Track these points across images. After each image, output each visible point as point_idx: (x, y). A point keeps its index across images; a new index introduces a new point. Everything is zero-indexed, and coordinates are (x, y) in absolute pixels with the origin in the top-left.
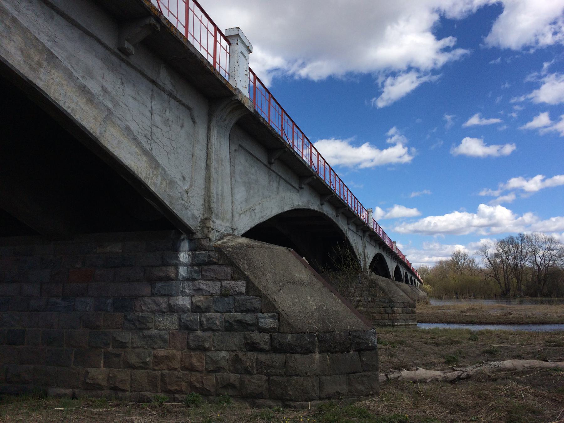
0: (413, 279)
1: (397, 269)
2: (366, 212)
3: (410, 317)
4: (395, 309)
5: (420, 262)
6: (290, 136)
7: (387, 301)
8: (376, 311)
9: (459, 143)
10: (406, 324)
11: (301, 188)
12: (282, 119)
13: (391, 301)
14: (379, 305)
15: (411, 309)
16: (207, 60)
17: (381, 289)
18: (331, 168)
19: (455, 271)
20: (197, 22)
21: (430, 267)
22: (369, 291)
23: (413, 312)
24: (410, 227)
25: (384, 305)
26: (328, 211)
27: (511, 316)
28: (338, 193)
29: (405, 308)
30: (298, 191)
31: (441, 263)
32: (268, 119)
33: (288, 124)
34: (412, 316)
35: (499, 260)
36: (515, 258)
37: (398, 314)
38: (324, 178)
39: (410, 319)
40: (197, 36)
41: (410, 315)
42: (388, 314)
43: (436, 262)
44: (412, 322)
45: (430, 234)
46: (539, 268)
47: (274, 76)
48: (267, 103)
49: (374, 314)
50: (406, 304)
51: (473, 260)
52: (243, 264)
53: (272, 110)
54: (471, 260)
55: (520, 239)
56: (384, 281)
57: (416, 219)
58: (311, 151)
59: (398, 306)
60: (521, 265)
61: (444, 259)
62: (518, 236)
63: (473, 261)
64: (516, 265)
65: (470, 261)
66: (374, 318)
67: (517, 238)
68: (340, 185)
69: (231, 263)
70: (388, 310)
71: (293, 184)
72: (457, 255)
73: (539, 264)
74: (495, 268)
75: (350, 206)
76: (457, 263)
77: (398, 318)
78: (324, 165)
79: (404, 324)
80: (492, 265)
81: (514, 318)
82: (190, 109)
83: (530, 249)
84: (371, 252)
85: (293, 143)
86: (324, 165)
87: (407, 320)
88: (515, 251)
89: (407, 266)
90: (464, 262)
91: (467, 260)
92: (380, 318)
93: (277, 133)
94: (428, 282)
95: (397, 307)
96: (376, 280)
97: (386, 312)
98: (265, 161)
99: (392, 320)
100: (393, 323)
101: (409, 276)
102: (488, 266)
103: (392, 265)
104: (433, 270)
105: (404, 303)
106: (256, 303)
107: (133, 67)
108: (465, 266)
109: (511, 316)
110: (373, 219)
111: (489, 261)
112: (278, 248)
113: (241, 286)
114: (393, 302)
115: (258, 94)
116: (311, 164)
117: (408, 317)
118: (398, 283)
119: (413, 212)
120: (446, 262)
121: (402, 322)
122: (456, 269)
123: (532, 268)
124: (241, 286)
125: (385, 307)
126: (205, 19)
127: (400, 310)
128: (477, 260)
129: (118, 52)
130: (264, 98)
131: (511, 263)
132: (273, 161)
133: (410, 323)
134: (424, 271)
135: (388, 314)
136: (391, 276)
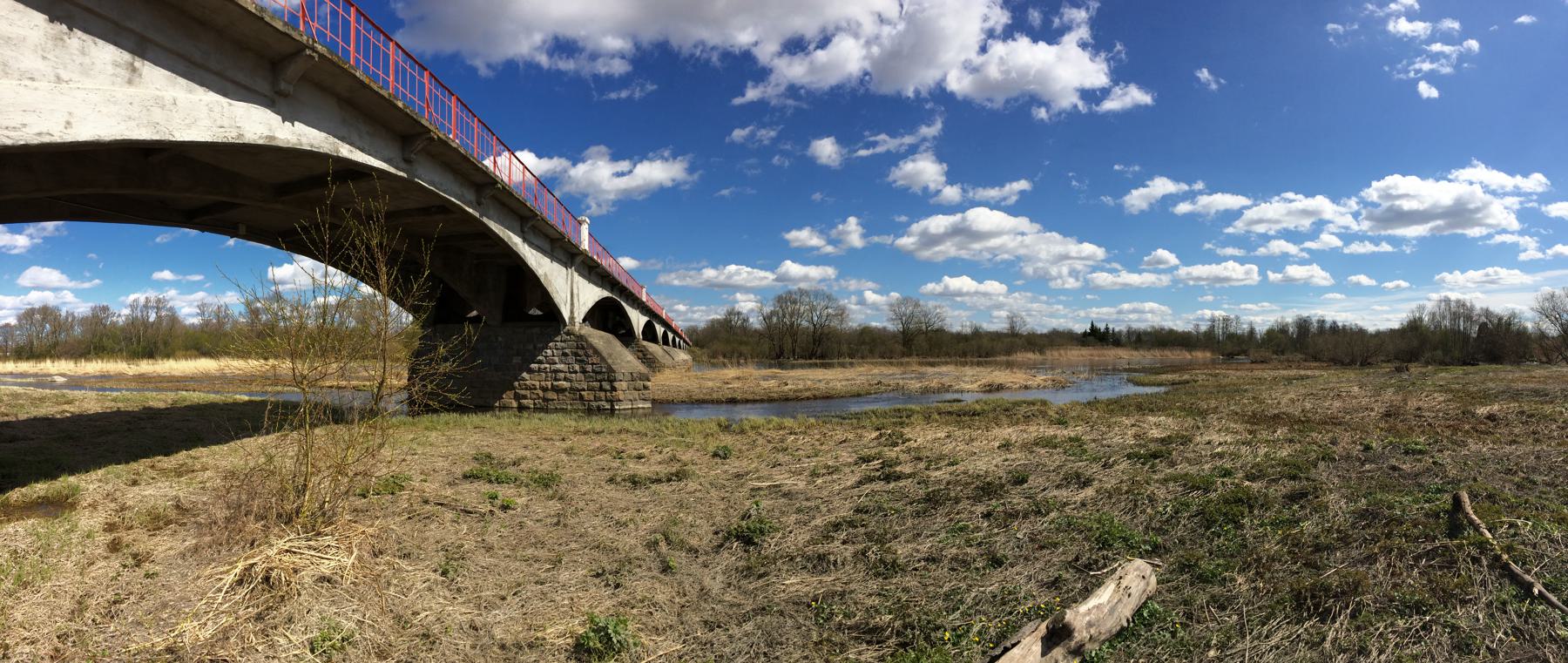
0: (677, 339)
1: (665, 333)
4: (616, 384)
7: (604, 370)
9: (730, 134)
13: (611, 370)
14: (591, 377)
17: (596, 352)
22: (576, 354)
23: (645, 388)
25: (599, 377)
26: (429, 180)
31: (713, 321)
35: (775, 320)
42: (606, 391)
47: (1071, 640)
49: (583, 393)
56: (602, 337)
61: (719, 317)
63: (746, 320)
66: (581, 397)
70: (606, 386)
84: (590, 294)
87: (636, 400)
92: (592, 398)
97: (601, 389)
99: (611, 402)
100: (612, 406)
101: (670, 336)
103: (660, 330)
104: (704, 330)
112: (891, 372)
114: (614, 372)
118: (665, 347)
120: (718, 321)
123: (808, 328)
125: (600, 381)
127: (624, 385)
128: (751, 320)
133: (640, 406)
135: (606, 391)
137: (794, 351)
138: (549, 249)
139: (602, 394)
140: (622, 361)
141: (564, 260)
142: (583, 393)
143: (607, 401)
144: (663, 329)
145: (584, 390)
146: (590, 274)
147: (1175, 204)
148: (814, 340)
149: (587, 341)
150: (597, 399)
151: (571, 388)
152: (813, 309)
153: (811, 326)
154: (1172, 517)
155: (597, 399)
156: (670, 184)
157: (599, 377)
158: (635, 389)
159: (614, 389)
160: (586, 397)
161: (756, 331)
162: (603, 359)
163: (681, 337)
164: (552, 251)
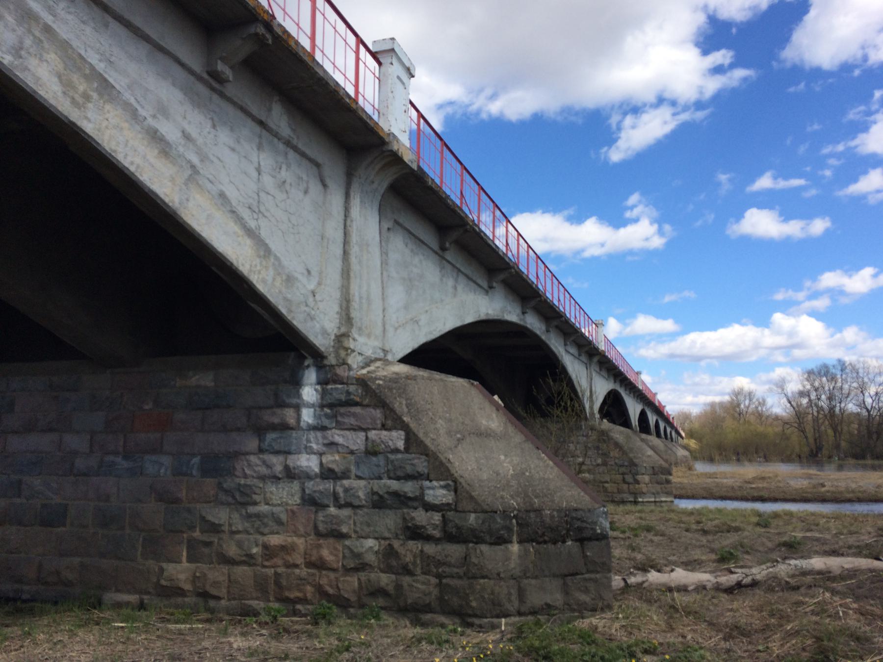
0: (669, 430)
1: (643, 415)
2: (594, 326)
3: (664, 489)
4: (639, 477)
5: (679, 404)
6: (473, 206)
7: (626, 464)
8: (609, 480)
10: (657, 500)
11: (491, 287)
12: (358, 59)
13: (633, 464)
15: (664, 477)
16: (344, 89)
18: (538, 257)
19: (734, 418)
20: (329, 30)
21: (695, 411)
22: (598, 448)
23: (668, 482)
24: (664, 349)
25: (622, 470)
27: (823, 489)
28: (549, 295)
29: (654, 475)
30: (487, 292)
31: (713, 405)
32: (309, 41)
33: (452, 166)
34: (666, 488)
35: (805, 401)
36: (830, 398)
37: (643, 485)
38: (442, 182)
39: (662, 493)
40: (329, 52)
41: (663, 486)
42: (629, 484)
43: (705, 404)
44: (666, 497)
45: (695, 360)
46: (869, 414)
48: (438, 155)
49: (606, 485)
50: (656, 469)
51: (764, 401)
52: (400, 406)
53: (447, 168)
54: (761, 400)
55: (839, 368)
56: (621, 433)
57: (672, 336)
58: (518, 244)
59: (643, 471)
60: (840, 410)
61: (717, 399)
62: (835, 363)
63: (763, 403)
64: (832, 409)
65: (760, 403)
66: (605, 490)
67: (834, 366)
68: (552, 283)
69: (382, 404)
70: (629, 478)
71: (480, 281)
72: (738, 393)
73: (869, 408)
74: (799, 415)
75: (568, 315)
76: (739, 405)
77: (644, 490)
78: (518, 240)
79: (653, 500)
80: (794, 408)
81: (828, 491)
82: (318, 165)
83: (855, 385)
84: (602, 387)
85: (479, 217)
86: (518, 240)
87: (658, 493)
88: (831, 387)
89: (659, 411)
90: (749, 404)
91: (754, 400)
92: (616, 490)
93: (454, 203)
94: (691, 434)
95: (643, 474)
96: (610, 430)
97: (624, 481)
98: (435, 245)
102: (787, 411)
103: (634, 408)
104: (699, 417)
105: (653, 468)
106: (421, 465)
107: (229, 100)
108: (750, 410)
109: (823, 489)
110: (605, 337)
111: (790, 403)
113: (397, 439)
114: (636, 465)
115: (424, 142)
116: (507, 249)
117: (659, 490)
118: (644, 436)
119: (668, 325)
120: (721, 404)
121: (650, 497)
122: (736, 415)
123: (858, 414)
124: (397, 439)
125: (623, 474)
126: (341, 26)
127: (647, 478)
128: (770, 401)
129: (205, 76)
130: (453, 172)
131: (825, 406)
132: (447, 245)
133: (663, 499)
134: (686, 417)
136: (634, 425)
137: (837, 447)
138: (577, 356)
139: (625, 486)
140: (643, 455)
141: (585, 361)
142: (606, 485)
143: (631, 493)
144: (655, 418)
145: (607, 482)
146: (601, 370)
147: (727, 61)
148: (870, 433)
149: (608, 436)
150: (620, 491)
151: (594, 480)
152: (862, 389)
153: (864, 411)
154: (872, 615)
155: (620, 491)
156: (819, 277)
157: (622, 470)
158: (658, 483)
159: (637, 482)
160: (610, 490)
161: (777, 418)
162: (624, 453)
163: (671, 425)
164: (580, 355)
